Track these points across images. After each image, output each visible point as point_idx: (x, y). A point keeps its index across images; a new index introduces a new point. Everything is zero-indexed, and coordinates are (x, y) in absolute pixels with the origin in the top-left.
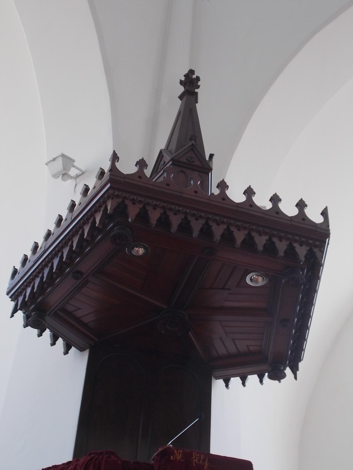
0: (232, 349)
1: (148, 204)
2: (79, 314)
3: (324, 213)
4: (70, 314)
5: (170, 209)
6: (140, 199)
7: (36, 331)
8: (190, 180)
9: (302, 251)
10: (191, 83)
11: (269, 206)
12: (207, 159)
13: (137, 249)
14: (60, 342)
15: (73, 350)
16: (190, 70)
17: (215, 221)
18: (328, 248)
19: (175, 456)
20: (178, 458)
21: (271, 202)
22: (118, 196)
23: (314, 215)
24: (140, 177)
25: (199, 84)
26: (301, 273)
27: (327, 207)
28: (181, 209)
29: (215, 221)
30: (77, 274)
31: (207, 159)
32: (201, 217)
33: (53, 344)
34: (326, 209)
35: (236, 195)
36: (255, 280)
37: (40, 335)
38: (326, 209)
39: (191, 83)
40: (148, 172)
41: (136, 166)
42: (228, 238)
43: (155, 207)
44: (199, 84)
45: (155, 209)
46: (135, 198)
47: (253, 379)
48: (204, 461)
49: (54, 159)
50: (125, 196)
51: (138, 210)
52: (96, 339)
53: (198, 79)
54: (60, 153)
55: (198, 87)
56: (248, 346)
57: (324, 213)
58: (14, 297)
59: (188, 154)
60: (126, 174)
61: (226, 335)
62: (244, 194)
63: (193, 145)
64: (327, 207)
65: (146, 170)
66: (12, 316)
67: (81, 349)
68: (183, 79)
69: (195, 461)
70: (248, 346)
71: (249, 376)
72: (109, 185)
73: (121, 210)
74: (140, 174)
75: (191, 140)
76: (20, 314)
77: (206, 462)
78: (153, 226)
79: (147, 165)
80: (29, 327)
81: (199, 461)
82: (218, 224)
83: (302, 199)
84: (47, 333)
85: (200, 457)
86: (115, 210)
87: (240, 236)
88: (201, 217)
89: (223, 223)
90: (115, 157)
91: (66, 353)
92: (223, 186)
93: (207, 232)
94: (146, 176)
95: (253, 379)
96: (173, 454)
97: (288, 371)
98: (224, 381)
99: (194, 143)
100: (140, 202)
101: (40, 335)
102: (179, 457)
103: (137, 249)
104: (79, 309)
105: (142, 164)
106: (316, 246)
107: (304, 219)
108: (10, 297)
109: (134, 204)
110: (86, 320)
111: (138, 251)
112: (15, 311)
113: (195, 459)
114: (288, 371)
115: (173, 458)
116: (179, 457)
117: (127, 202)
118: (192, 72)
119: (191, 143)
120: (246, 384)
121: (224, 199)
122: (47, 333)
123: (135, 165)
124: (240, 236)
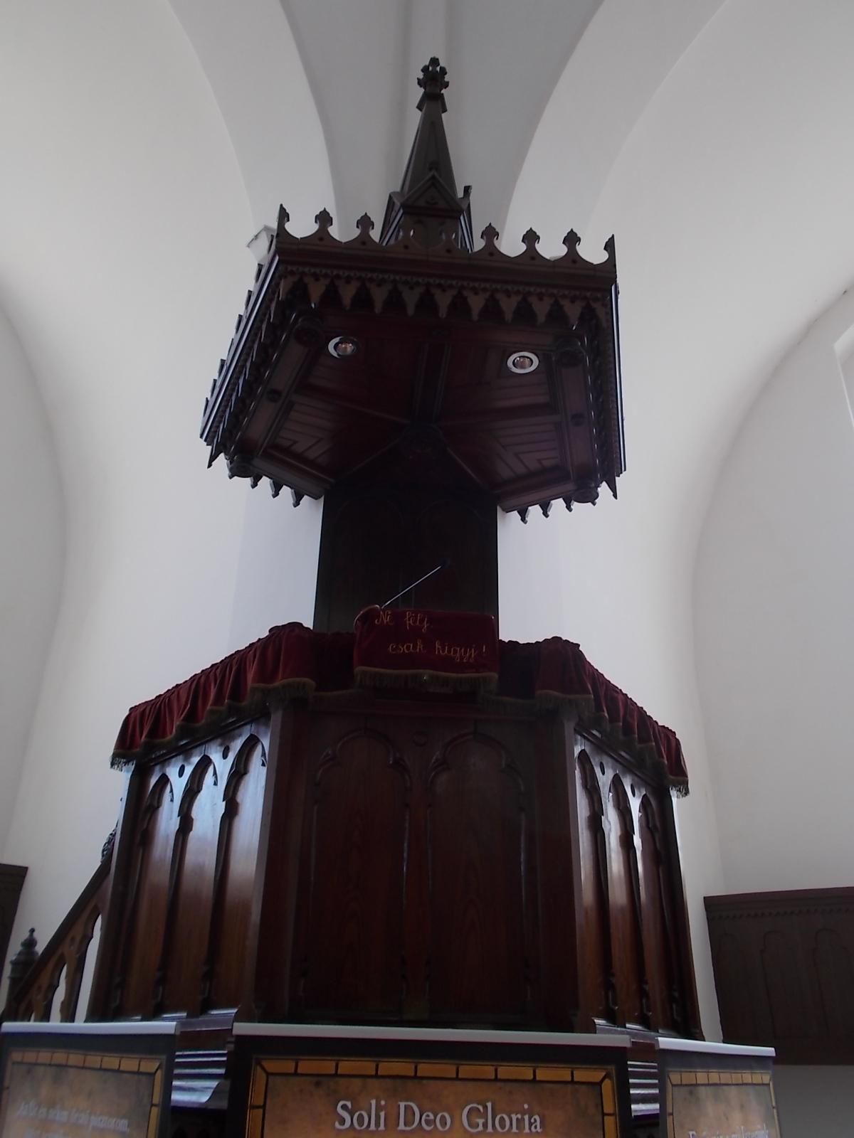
0: (521, 470)
1: (338, 277)
2: (299, 448)
3: (610, 246)
4: (287, 451)
5: (564, 296)
6: (483, 285)
7: (248, 481)
8: (441, 234)
9: (573, 311)
10: (434, 81)
11: (562, 251)
12: (460, 194)
13: (344, 346)
14: (286, 492)
15: (306, 499)
16: (431, 59)
17: (439, 286)
18: (619, 300)
19: (381, 620)
20: (385, 621)
21: (524, 243)
22: (292, 273)
23: (592, 253)
24: (364, 243)
25: (446, 80)
26: (579, 344)
27: (281, 205)
28: (386, 276)
29: (439, 286)
30: (274, 394)
31: (460, 194)
32: (418, 284)
33: (276, 494)
34: (612, 239)
35: (511, 246)
36: (524, 363)
37: (254, 485)
38: (612, 239)
39: (434, 81)
40: (375, 234)
41: (482, 237)
42: (492, 311)
43: (348, 280)
44: (446, 80)
45: (379, 285)
46: (397, 278)
47: (558, 505)
48: (422, 621)
49: (256, 237)
50: (292, 271)
51: (324, 288)
52: (332, 480)
53: (443, 71)
54: (261, 227)
55: (446, 85)
56: (539, 461)
57: (610, 246)
58: (209, 441)
59: (431, 192)
60: (301, 238)
61: (520, 448)
62: (564, 243)
63: (433, 177)
64: (613, 236)
65: (373, 231)
66: (210, 465)
67: (315, 497)
68: (421, 76)
69: (410, 624)
70: (539, 461)
71: (553, 502)
72: (277, 258)
73: (299, 293)
74: (364, 239)
75: (430, 169)
76: (222, 460)
77: (425, 622)
78: (348, 308)
79: (373, 224)
80: (236, 477)
81: (415, 622)
82: (444, 290)
83: (572, 230)
84: (265, 482)
85: (416, 616)
86: (291, 292)
87: (508, 306)
88: (418, 284)
89: (451, 287)
90: (284, 215)
91: (297, 504)
92: (491, 233)
93: (460, 305)
94: (582, 259)
95: (558, 505)
96: (378, 616)
97: (604, 489)
98: (519, 512)
99: (436, 174)
100: (326, 276)
101: (254, 485)
102: (386, 620)
103: (344, 346)
104: (295, 442)
105: (365, 222)
106: (596, 299)
107: (574, 262)
108: (205, 441)
109: (476, 294)
110: (312, 455)
111: (346, 348)
112: (213, 458)
113: (409, 620)
114: (604, 489)
115: (378, 621)
116: (386, 620)
117: (306, 280)
118: (434, 61)
119: (431, 174)
120: (549, 513)
121: (533, 258)
122: (265, 482)
123: (603, 247)
124: (508, 306)
